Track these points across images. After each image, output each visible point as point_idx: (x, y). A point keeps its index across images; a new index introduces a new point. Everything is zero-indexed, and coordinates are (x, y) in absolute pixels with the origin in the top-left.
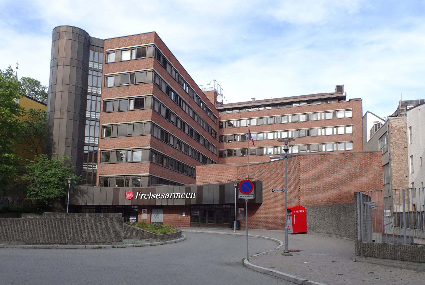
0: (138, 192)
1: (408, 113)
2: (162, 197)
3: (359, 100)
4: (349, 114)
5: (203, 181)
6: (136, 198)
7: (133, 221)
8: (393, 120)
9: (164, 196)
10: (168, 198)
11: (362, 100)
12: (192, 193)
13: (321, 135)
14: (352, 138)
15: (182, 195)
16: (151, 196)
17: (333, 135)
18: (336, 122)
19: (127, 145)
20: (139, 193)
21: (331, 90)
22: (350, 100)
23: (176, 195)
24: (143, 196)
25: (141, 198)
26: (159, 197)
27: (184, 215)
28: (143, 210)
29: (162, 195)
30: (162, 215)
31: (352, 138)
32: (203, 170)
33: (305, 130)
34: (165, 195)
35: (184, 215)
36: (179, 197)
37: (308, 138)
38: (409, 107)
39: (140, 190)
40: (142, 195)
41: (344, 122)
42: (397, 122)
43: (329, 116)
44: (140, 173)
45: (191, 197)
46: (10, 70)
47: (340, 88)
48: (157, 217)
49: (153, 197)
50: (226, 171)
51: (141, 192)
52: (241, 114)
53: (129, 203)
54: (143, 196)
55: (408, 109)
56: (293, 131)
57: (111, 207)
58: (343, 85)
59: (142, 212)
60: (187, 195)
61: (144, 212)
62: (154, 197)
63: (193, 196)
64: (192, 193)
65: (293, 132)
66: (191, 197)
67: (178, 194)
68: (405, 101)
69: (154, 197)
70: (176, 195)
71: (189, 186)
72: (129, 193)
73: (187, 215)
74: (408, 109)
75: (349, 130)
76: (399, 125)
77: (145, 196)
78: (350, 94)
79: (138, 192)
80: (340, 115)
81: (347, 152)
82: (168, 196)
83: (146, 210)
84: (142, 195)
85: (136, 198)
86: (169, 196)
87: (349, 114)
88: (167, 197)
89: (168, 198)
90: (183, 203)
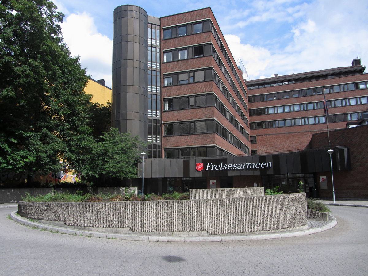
0: (208, 164)
2: (235, 168)
5: (265, 151)
6: (207, 169)
9: (236, 167)
12: (268, 163)
15: (256, 165)
16: (223, 167)
20: (210, 164)
21: (348, 64)
23: (250, 165)
24: (214, 167)
25: (212, 169)
26: (264, 166)
29: (234, 166)
34: (237, 166)
36: (253, 167)
39: (210, 161)
45: (267, 167)
46: (276, 75)
47: (357, 62)
49: (224, 168)
51: (211, 163)
53: (199, 175)
54: (214, 167)
57: (178, 180)
58: (360, 59)
62: (226, 168)
63: (269, 165)
64: (268, 163)
65: (319, 104)
66: (267, 167)
67: (251, 164)
69: (226, 168)
70: (250, 165)
71: (188, 159)
77: (216, 167)
81: (353, 122)
82: (241, 166)
85: (207, 169)
88: (240, 167)
89: (241, 168)
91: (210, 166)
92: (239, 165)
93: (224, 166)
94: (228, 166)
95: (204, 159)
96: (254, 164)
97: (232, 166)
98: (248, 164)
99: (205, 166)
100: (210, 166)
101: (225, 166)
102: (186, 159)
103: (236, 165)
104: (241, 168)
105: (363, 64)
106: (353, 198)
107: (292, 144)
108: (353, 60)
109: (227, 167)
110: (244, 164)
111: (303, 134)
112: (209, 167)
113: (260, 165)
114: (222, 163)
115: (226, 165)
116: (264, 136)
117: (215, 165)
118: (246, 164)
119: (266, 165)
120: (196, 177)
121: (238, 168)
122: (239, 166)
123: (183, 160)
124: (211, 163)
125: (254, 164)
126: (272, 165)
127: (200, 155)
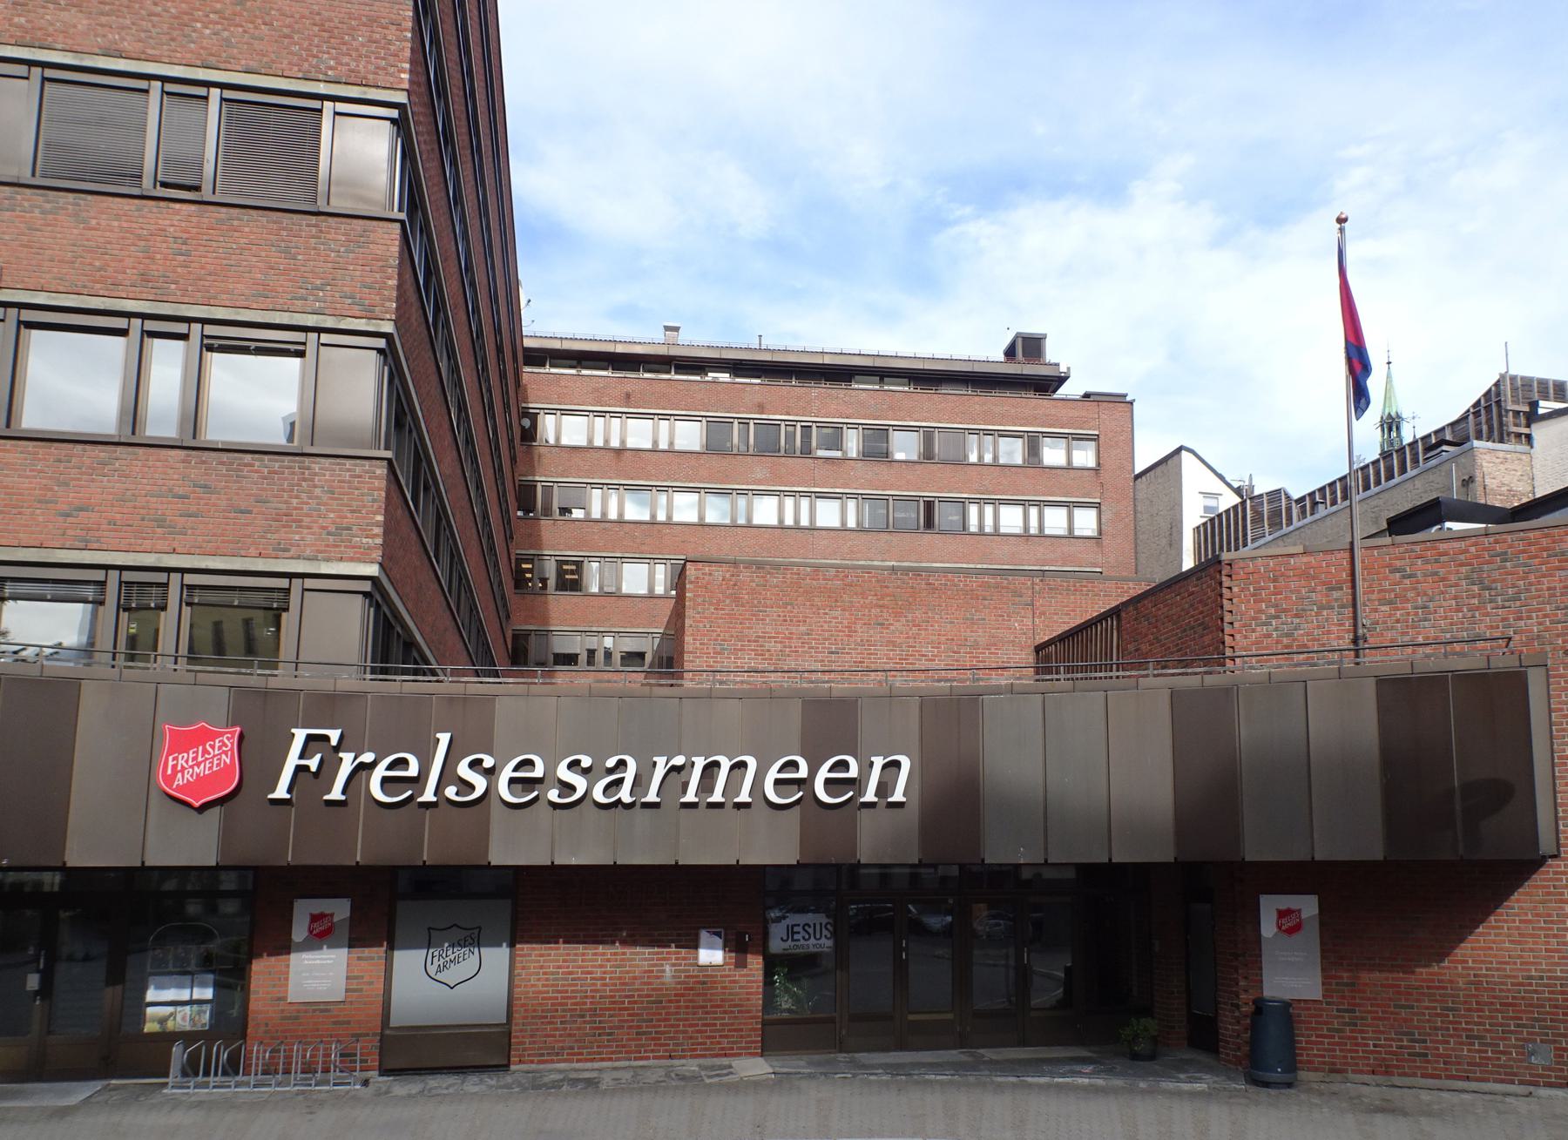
1: (1538, 431)
2: (568, 788)
3: (1120, 402)
4: (1085, 457)
6: (281, 792)
7: (182, 1020)
8: (1487, 457)
9: (580, 783)
10: (625, 795)
11: (1131, 403)
13: (981, 533)
14: (1099, 558)
15: (773, 774)
17: (1026, 536)
18: (1033, 482)
19: (145, 278)
21: (988, 350)
22: (1087, 395)
25: (336, 794)
27: (711, 955)
28: (303, 911)
30: (496, 958)
31: (1099, 558)
32: (736, 600)
33: (915, 499)
35: (711, 955)
37: (927, 538)
38: (1545, 407)
40: (347, 762)
41: (1066, 488)
42: (1502, 467)
43: (1012, 452)
44: (281, 551)
47: (1030, 346)
48: (450, 976)
50: (898, 615)
51: (334, 735)
52: (629, 387)
54: (364, 769)
55: (1541, 411)
56: (865, 497)
58: (1045, 337)
59: (299, 933)
60: (823, 773)
61: (322, 935)
63: (884, 789)
64: (879, 762)
66: (870, 796)
67: (726, 764)
68: (1523, 378)
72: (203, 737)
73: (737, 946)
74: (1541, 411)
75: (1086, 521)
76: (1506, 480)
77: (380, 772)
78: (1084, 368)
79: (300, 735)
80: (1053, 455)
82: (629, 776)
83: (340, 909)
84: (347, 762)
86: (640, 783)
87: (1085, 457)
90: (775, 847)
91: (313, 764)
92: (611, 763)
93: (463, 770)
94: (507, 773)
95: (1192, 682)
96: (752, 762)
97: (538, 772)
98: (700, 762)
99: (258, 755)
100: (313, 764)
101: (475, 765)
102: (648, 658)
103: (586, 762)
104: (625, 795)
105: (1053, 353)
106: (1550, 1085)
107: (929, 650)
108: (1018, 336)
109: (490, 773)
110: (661, 761)
111: (997, 586)
112: (300, 769)
113: (803, 772)
114: (444, 738)
115: (488, 762)
116: (745, 575)
117: (368, 757)
118: (679, 760)
119: (418, 781)
120: (144, 869)
121: (598, 795)
122: (610, 771)
123: (1175, 695)
124: (334, 735)
125: (752, 762)
126: (916, 786)
127: (211, 647)
